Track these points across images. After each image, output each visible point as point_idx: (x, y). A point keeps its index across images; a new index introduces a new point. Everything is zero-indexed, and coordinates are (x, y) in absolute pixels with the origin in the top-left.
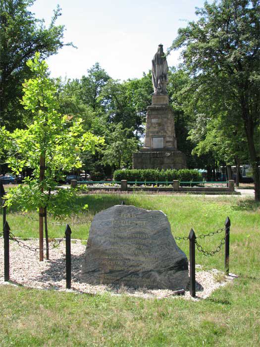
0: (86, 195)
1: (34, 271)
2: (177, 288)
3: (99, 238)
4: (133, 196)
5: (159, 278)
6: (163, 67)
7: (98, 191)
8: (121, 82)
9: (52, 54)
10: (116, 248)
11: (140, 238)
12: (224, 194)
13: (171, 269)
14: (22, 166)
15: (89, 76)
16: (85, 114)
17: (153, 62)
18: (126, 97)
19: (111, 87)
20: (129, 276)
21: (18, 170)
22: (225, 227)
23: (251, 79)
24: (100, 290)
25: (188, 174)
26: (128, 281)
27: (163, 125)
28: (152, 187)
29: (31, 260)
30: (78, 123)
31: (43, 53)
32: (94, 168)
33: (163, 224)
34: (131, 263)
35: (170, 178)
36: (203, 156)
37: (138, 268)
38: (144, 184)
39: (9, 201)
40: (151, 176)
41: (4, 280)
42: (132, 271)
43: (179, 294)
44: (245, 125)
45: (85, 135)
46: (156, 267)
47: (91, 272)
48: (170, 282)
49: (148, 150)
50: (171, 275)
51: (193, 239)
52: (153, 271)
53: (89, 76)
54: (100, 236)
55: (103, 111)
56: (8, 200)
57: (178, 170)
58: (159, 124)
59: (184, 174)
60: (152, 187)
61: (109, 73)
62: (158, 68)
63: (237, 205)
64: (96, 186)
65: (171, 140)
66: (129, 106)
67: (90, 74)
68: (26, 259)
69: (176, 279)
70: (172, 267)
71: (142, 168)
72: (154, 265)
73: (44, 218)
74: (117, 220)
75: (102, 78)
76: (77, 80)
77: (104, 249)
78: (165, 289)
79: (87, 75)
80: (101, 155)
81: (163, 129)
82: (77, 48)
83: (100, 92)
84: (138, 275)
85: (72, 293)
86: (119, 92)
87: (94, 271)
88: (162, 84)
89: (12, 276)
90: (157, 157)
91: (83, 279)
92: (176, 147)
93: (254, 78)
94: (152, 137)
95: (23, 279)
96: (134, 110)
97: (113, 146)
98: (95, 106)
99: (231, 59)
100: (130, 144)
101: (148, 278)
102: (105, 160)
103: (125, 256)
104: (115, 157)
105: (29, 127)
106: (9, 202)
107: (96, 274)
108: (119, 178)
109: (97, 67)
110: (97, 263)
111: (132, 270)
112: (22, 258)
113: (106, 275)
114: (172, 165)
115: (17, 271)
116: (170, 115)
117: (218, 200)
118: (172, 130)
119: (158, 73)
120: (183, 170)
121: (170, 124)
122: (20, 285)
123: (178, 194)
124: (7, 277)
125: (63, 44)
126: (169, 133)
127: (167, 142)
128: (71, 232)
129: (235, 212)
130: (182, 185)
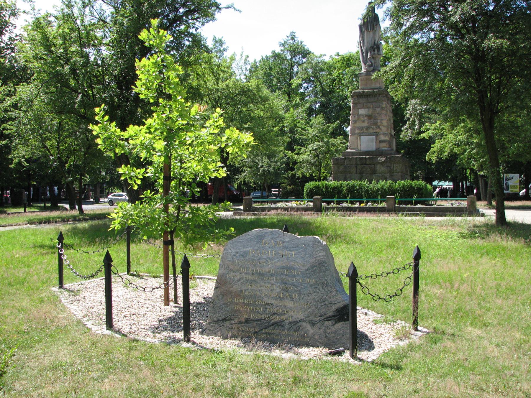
0: (257, 217)
1: (151, 318)
2: (336, 347)
3: (231, 275)
4: (323, 219)
5: (311, 331)
6: (374, 35)
7: (273, 212)
8: (327, 59)
9: (207, 22)
10: (256, 288)
11: (287, 275)
12: (453, 215)
13: (328, 319)
14: (141, 177)
15: (282, 50)
16: (269, 104)
17: (361, 27)
18: (334, 80)
19: (312, 66)
20: (271, 328)
21: (135, 182)
22: (413, 261)
23: (486, 44)
24: (230, 346)
25: (411, 187)
26: (269, 334)
27: (375, 118)
28: (357, 205)
29: (153, 304)
30: (215, 115)
31: (195, 21)
32: (286, 181)
33: (319, 256)
34: (275, 310)
35: (384, 193)
36: (440, 160)
37: (283, 317)
38: (347, 202)
39: (117, 222)
40: (357, 190)
41: (106, 328)
42: (276, 320)
43: (334, 354)
44: (482, 114)
45: (228, 132)
46: (308, 317)
47: (220, 321)
48: (326, 337)
49: (352, 154)
50: (328, 327)
51: (354, 276)
52: (304, 321)
53: (282, 50)
54: (234, 272)
55: (301, 100)
56: (115, 220)
57: (396, 182)
58: (370, 117)
59: (403, 187)
60: (357, 205)
61: (310, 45)
62: (367, 35)
63: (467, 232)
64: (279, 205)
65: (387, 138)
66: (339, 92)
67: (283, 48)
68: (147, 302)
69: (335, 333)
70: (330, 317)
71: (345, 179)
72: (306, 312)
73: (170, 247)
74: (257, 250)
75: (299, 53)
76: (267, 57)
77: (239, 289)
78: (318, 347)
79: (278, 50)
80: (293, 163)
81: (375, 124)
82: (240, 12)
83: (297, 73)
84: (283, 326)
85: (189, 348)
86: (323, 73)
87: (224, 320)
88: (373, 58)
89: (117, 323)
90: (366, 164)
91: (210, 330)
92: (394, 148)
93: (490, 43)
94: (360, 135)
95: (131, 328)
96: (346, 98)
97: (310, 149)
98: (290, 93)
99: (457, 17)
100: (334, 145)
101: (296, 331)
102: (299, 170)
103: (266, 300)
104: (313, 164)
105: (146, 122)
106: (117, 223)
107: (227, 324)
108: (311, 194)
109: (293, 39)
110: (228, 308)
111: (275, 319)
112: (142, 301)
113: (240, 325)
114: (388, 175)
115: (128, 318)
116: (384, 103)
117: (441, 225)
118: (388, 125)
119: (367, 43)
120: (403, 182)
121: (386, 115)
122: (125, 335)
123: (386, 215)
124: (110, 324)
125: (220, 7)
126: (384, 129)
127: (381, 142)
128: (189, 266)
129: (461, 240)
130: (400, 203)
